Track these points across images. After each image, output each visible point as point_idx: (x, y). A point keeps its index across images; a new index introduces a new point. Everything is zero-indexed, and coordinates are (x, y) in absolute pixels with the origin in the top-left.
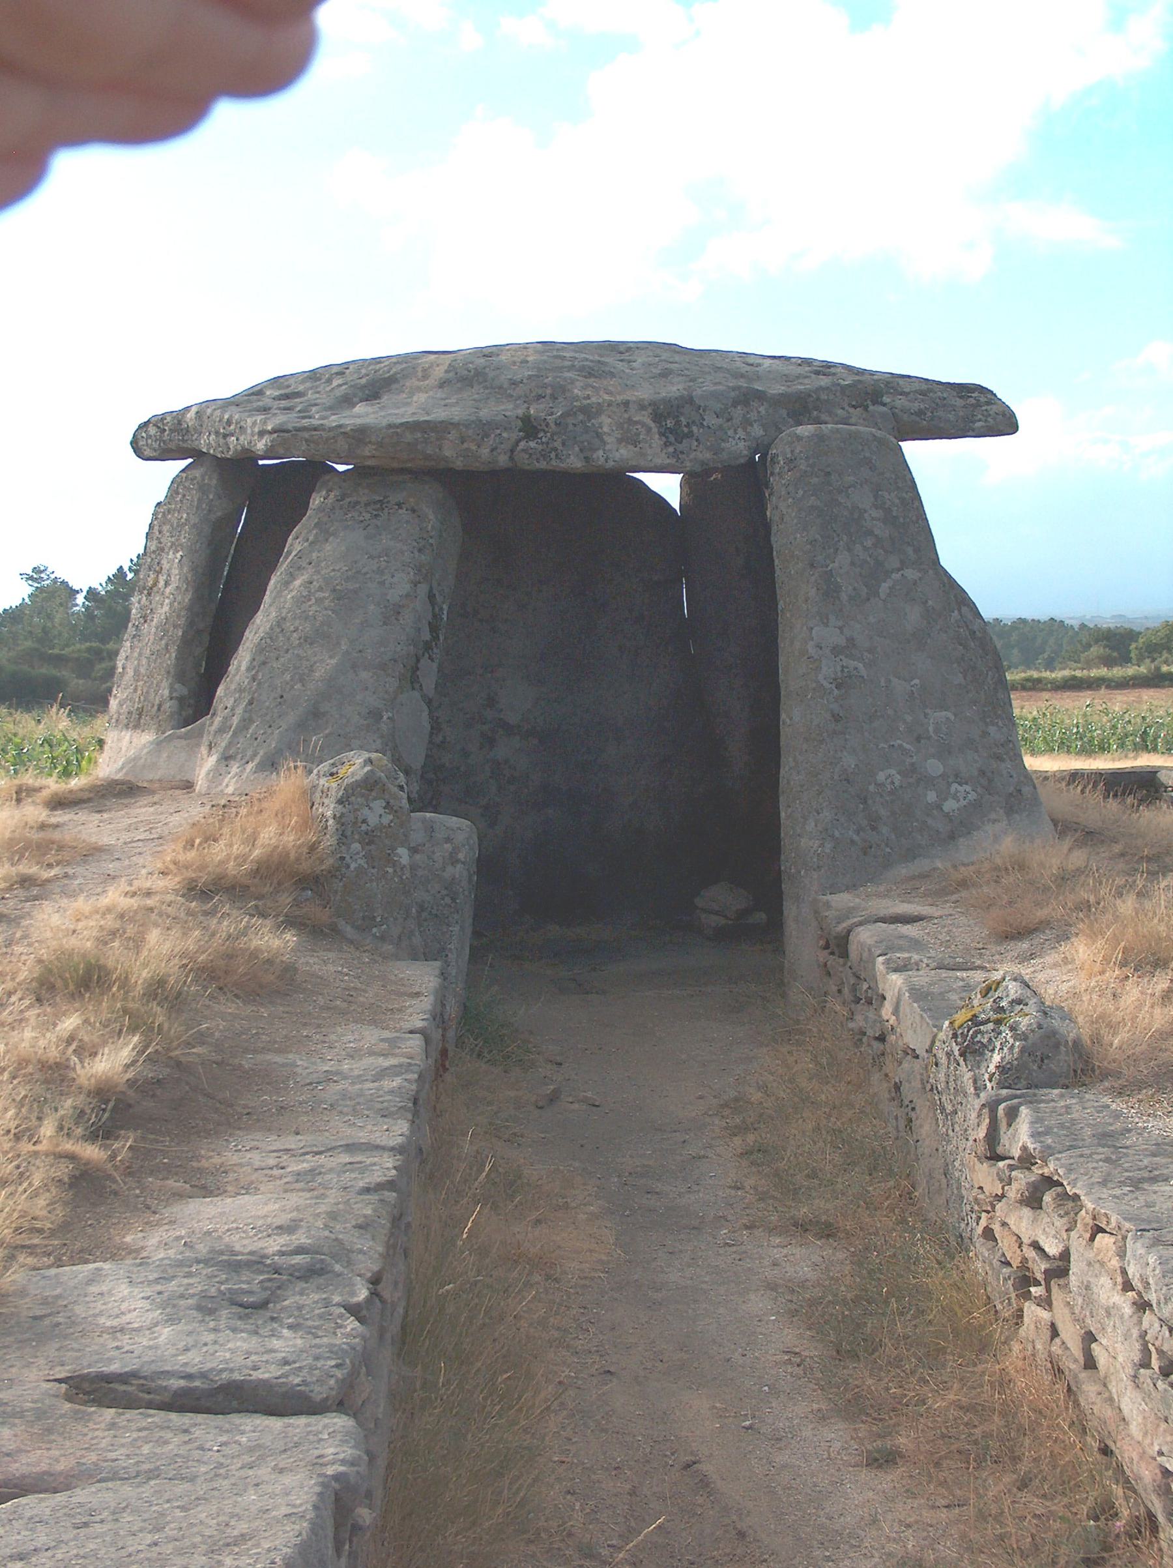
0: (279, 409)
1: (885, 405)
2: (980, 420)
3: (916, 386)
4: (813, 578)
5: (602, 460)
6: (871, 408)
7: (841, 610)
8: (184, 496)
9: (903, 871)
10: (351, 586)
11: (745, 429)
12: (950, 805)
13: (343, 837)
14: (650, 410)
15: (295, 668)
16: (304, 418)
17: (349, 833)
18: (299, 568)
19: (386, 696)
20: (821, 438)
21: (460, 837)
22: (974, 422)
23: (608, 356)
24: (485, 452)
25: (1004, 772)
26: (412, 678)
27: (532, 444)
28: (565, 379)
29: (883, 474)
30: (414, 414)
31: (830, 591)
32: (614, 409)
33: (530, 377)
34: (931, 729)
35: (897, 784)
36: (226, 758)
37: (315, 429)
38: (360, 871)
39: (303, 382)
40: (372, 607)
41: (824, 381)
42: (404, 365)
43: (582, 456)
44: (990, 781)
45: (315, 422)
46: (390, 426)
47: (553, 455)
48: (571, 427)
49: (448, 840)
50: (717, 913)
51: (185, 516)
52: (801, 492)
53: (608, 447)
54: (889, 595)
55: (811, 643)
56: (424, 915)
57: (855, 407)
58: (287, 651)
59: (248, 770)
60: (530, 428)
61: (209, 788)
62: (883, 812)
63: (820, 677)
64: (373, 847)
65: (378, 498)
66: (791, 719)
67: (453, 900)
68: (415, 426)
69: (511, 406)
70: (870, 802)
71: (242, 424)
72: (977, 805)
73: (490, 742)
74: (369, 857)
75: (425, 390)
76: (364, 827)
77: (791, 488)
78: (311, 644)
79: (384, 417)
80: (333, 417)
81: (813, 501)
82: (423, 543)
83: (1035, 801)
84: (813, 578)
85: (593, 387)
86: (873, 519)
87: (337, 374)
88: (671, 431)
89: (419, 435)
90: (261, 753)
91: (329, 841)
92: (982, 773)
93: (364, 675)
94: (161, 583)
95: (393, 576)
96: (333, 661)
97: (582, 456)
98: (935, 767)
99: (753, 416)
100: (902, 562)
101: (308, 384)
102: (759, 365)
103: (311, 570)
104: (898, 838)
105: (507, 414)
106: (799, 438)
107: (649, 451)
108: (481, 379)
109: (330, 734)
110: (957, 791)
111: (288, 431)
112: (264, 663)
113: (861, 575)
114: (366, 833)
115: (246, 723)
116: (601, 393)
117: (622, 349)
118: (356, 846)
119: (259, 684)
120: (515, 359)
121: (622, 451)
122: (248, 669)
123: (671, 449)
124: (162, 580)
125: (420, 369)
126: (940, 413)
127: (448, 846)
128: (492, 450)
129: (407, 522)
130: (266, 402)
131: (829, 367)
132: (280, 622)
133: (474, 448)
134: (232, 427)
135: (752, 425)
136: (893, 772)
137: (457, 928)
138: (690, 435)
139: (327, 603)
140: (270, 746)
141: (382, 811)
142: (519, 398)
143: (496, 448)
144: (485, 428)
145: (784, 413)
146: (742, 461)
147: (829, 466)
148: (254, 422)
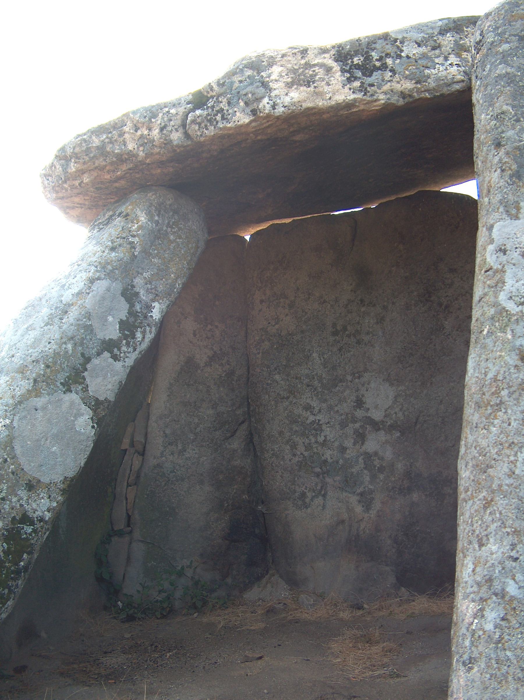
5: (268, 107)
11: (458, 55)
24: (156, 132)
47: (219, 117)
48: (237, 85)
53: (273, 94)
81: (502, 69)
97: (248, 110)
128: (162, 129)
133: (146, 132)
138: (384, 67)
143: (165, 127)
146: (457, 87)
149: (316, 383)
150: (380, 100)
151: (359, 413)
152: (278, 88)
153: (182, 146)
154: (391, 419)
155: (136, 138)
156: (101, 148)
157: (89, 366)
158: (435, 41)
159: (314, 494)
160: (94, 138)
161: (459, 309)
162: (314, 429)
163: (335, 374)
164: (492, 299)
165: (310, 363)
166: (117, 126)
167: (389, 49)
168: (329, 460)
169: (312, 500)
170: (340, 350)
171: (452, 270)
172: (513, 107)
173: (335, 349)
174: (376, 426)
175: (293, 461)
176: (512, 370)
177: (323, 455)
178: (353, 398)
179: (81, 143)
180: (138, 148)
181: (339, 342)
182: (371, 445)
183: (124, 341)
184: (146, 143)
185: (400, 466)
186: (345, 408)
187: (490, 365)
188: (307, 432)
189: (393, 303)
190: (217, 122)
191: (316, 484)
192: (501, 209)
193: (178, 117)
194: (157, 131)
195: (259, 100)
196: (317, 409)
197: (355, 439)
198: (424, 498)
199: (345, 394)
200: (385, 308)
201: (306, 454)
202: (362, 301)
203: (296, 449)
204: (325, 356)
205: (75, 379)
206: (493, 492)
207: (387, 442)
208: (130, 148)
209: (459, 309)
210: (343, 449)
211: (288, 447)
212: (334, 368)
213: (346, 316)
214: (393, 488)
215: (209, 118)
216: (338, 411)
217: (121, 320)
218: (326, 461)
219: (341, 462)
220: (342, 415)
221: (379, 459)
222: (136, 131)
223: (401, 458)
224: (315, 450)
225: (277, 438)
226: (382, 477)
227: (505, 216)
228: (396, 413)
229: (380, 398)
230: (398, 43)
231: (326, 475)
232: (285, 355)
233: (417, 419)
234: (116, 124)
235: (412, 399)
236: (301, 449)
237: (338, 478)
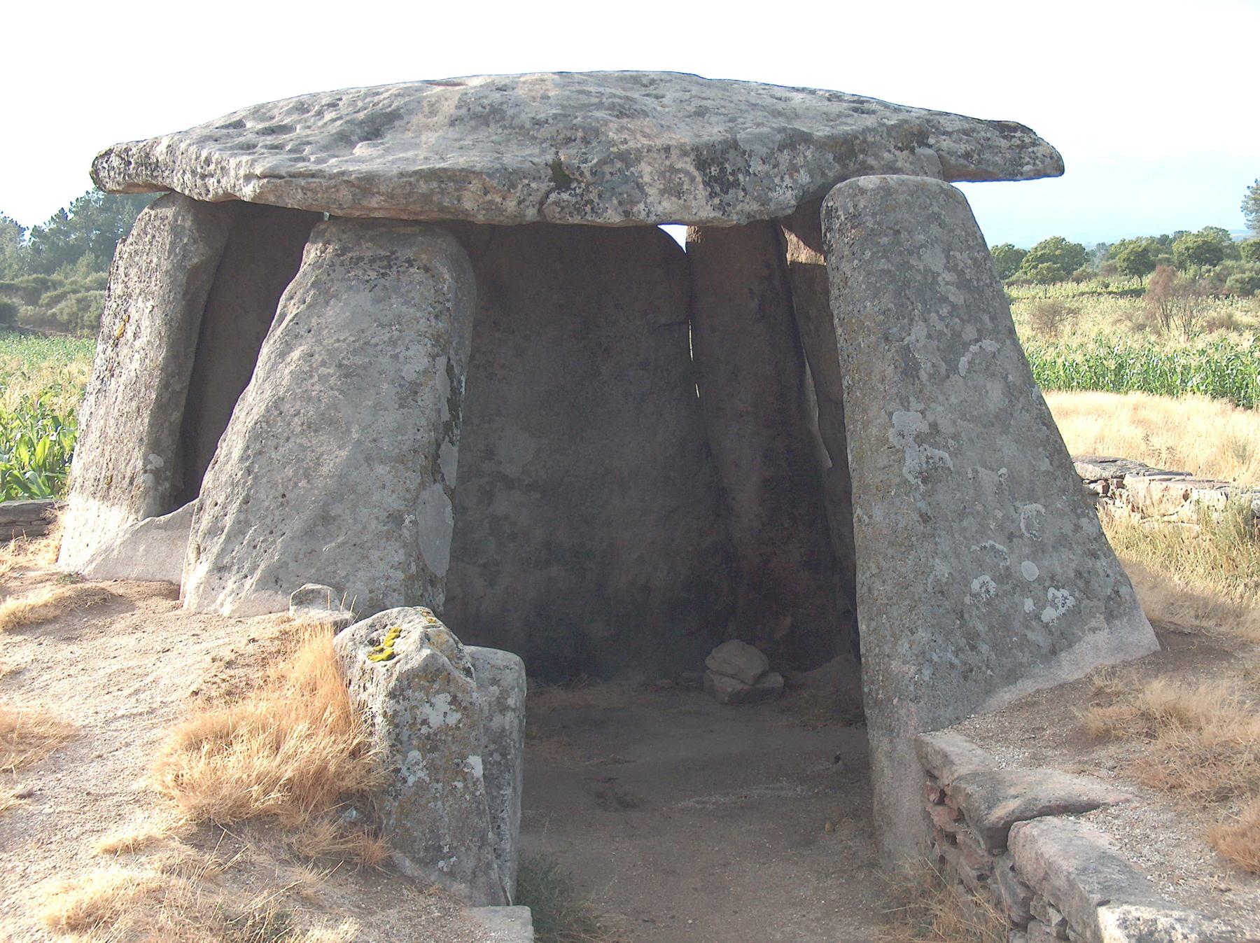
0: (266, 147)
1: (930, 146)
2: (1028, 163)
3: (958, 125)
4: (889, 355)
5: (643, 214)
6: (917, 150)
7: (921, 391)
8: (154, 237)
9: (1007, 696)
10: (359, 360)
11: (791, 177)
12: (1049, 614)
13: (397, 744)
14: (692, 156)
15: (299, 461)
16: (296, 160)
17: (405, 738)
18: (296, 336)
19: (408, 496)
20: (887, 191)
22: (1022, 165)
23: (633, 89)
24: (511, 205)
25: (1100, 571)
26: (434, 471)
27: (565, 196)
28: (597, 120)
29: (953, 230)
30: (426, 158)
31: (909, 370)
32: (655, 155)
33: (555, 117)
34: (1022, 525)
35: (992, 591)
36: (220, 569)
37: (313, 176)
38: (420, 784)
39: (289, 113)
40: (385, 386)
41: (869, 121)
42: (407, 99)
44: (1087, 583)
45: (314, 167)
46: (402, 175)
47: (588, 208)
48: (608, 176)
49: (494, 681)
50: (732, 676)
51: (155, 260)
52: (868, 254)
54: (969, 371)
55: (891, 430)
57: (901, 149)
58: (288, 439)
59: (247, 586)
60: (561, 177)
61: (199, 606)
62: (981, 628)
64: (436, 754)
65: (383, 253)
66: (870, 517)
67: (504, 755)
68: (433, 175)
69: (537, 151)
70: (966, 616)
71: (224, 164)
72: (1075, 614)
73: (487, 496)
74: (432, 769)
75: (434, 128)
76: (424, 730)
77: (855, 249)
78: (316, 431)
79: (393, 162)
80: (333, 161)
81: (883, 264)
82: (439, 307)
83: (1134, 604)
84: (889, 355)
85: (628, 129)
86: (947, 283)
87: (329, 105)
88: (716, 179)
89: (435, 185)
90: (262, 567)
91: (380, 746)
92: (1079, 574)
93: (380, 470)
94: (129, 335)
95: (407, 349)
96: (344, 453)
97: (620, 210)
98: (1029, 570)
99: (800, 161)
100: (979, 331)
101: (295, 117)
102: (787, 99)
103: (310, 339)
104: (989, 657)
105: (536, 160)
106: (863, 191)
107: (694, 203)
108: (498, 117)
109: (344, 543)
110: (1055, 597)
111: (281, 177)
112: (260, 453)
113: (938, 349)
114: (428, 738)
115: (241, 527)
116: (638, 136)
117: (645, 81)
118: (415, 755)
119: (255, 478)
120: (534, 93)
121: (664, 204)
122: (243, 459)
123: (717, 201)
124: (130, 330)
125: (425, 103)
126: (987, 156)
127: (494, 689)
128: (520, 203)
129: (421, 283)
130: (249, 137)
131: (862, 102)
132: (278, 403)
133: (498, 200)
134: (212, 167)
135: (798, 171)
136: (987, 578)
139: (332, 381)
140: (272, 557)
141: (446, 708)
142: (545, 140)
143: (524, 200)
144: (511, 178)
145: (830, 157)
146: (789, 211)
147: (896, 224)
148: (238, 164)
156: (426, 198)
160: (421, 183)
164: (897, 471)
174: (510, 484)
182: (502, 506)
194: (514, 203)
222: (485, 194)
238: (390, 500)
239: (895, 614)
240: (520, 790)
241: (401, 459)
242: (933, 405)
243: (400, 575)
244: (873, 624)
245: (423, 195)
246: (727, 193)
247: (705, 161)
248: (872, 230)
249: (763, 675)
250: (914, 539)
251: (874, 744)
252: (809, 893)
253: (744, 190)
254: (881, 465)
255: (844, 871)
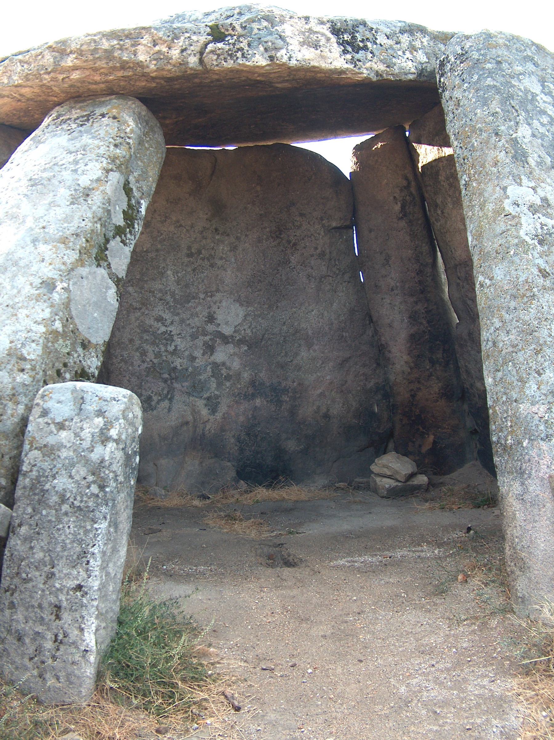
11: (411, 53)
14: (328, 25)
19: (63, 267)
21: (115, 409)
24: (175, 53)
27: (220, 45)
43: (266, 55)
47: (239, 54)
48: (256, 31)
49: (100, 413)
50: (389, 477)
52: (476, 77)
53: (290, 48)
56: (65, 507)
63: (522, 233)
67: (102, 488)
73: (210, 349)
84: (500, 144)
86: (544, 102)
88: (348, 43)
93: (43, 248)
97: (266, 55)
99: (417, 44)
123: (349, 57)
127: (99, 421)
128: (182, 51)
133: (165, 49)
137: (103, 526)
138: (365, 48)
143: (185, 49)
147: (498, 56)
149: (168, 298)
150: (363, 73)
151: (210, 328)
152: (294, 44)
153: (195, 70)
154: (240, 334)
155: (152, 52)
157: (108, 246)
158: (398, 37)
159: (160, 398)
160: (104, 40)
161: (304, 248)
162: (165, 339)
163: (188, 291)
165: (165, 279)
166: (133, 36)
167: (368, 35)
168: (179, 367)
169: (158, 402)
170: (194, 270)
171: (302, 215)
172: (502, 110)
173: (189, 270)
174: (225, 339)
175: (141, 367)
176: (536, 277)
177: (172, 363)
178: (205, 313)
179: (90, 42)
180: (150, 61)
181: (193, 263)
182: (220, 356)
183: (128, 230)
184: (161, 59)
185: (246, 376)
186: (196, 322)
187: (521, 273)
188: (157, 341)
189: (246, 235)
190: (237, 58)
191: (163, 389)
192: (511, 178)
193: (199, 44)
194: (178, 51)
195: (277, 49)
196: (169, 322)
197: (204, 350)
198: (265, 403)
199: (197, 310)
200: (238, 238)
201: (156, 361)
202: (216, 230)
203: (146, 356)
204: (179, 275)
205: (101, 257)
206: (541, 345)
207: (235, 354)
208: (141, 59)
209: (304, 248)
210: (193, 359)
211: (138, 354)
212: (187, 286)
213: (201, 241)
214: (239, 394)
215: (230, 52)
216: (189, 324)
217: (124, 210)
218: (175, 368)
219: (190, 369)
220: (193, 328)
221: (226, 368)
222: (154, 46)
223: (247, 369)
224: (164, 358)
225: (127, 345)
226: (228, 384)
227: (513, 183)
228: (245, 330)
229: (231, 316)
230: (373, 32)
231: (174, 381)
232: (139, 269)
233: (263, 336)
234: (131, 34)
235: (260, 319)
236: (151, 356)
237: (186, 384)
238: (46, 270)
239: (521, 359)
240: (125, 525)
241: (64, 241)
242: (542, 184)
243: (42, 329)
244: (500, 374)
245: (106, 51)
246: (357, 53)
247: (339, 30)
248: (478, 60)
249: (412, 475)
250: (535, 290)
251: (503, 490)
252: (440, 640)
253: (371, 53)
254: (498, 230)
255: (476, 618)
